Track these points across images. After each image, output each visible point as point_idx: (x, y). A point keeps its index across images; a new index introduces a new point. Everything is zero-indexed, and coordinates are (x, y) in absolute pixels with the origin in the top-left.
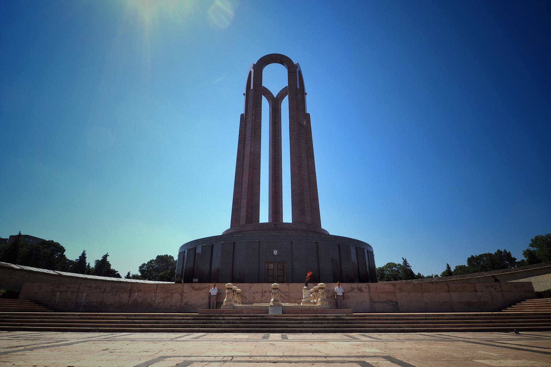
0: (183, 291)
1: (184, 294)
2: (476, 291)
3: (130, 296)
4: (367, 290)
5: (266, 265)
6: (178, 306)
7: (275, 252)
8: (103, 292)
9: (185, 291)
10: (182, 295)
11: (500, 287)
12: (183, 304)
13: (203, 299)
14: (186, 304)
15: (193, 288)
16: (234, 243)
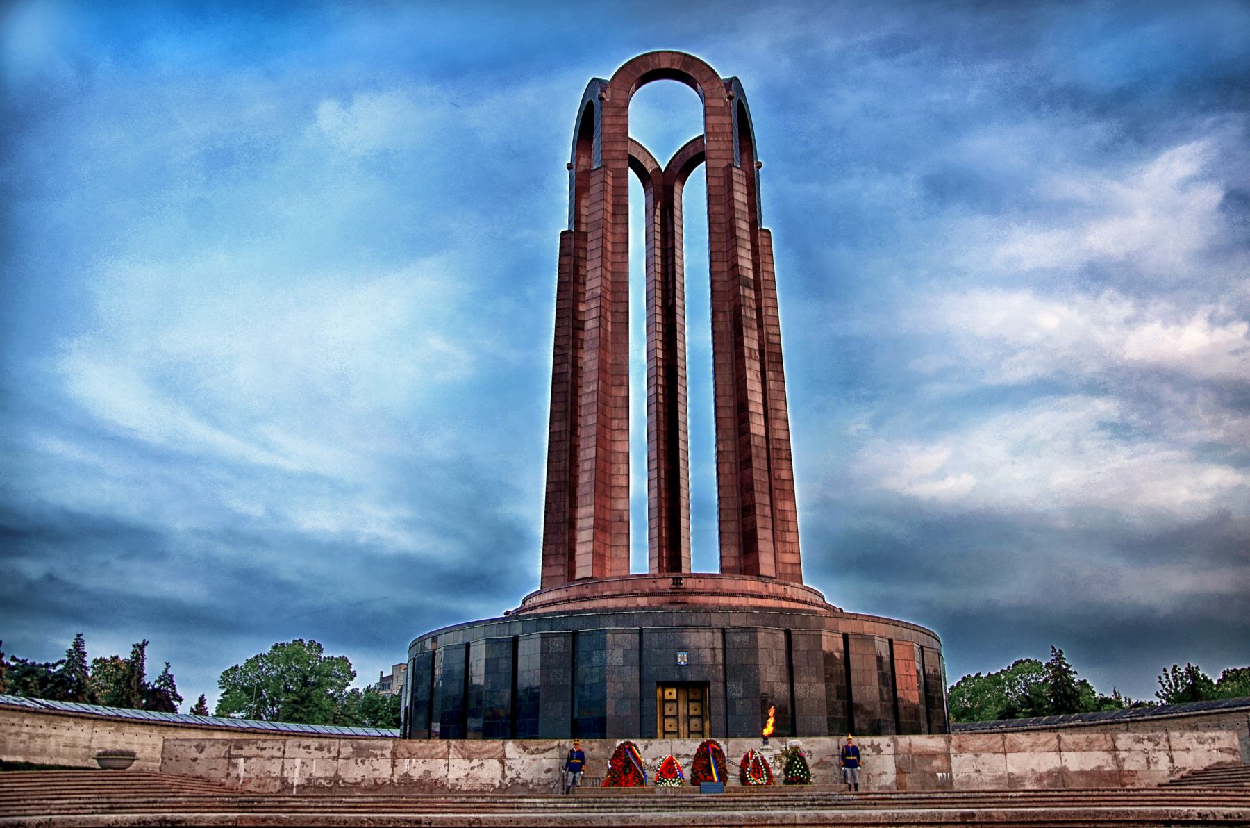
0: (504, 756)
1: (508, 763)
2: (1115, 749)
3: (394, 766)
4: (891, 750)
5: (659, 692)
6: (497, 785)
7: (682, 658)
8: (336, 758)
9: (508, 756)
10: (502, 762)
11: (1168, 740)
12: (507, 781)
13: (548, 771)
14: (512, 780)
15: (525, 748)
16: (575, 634)
